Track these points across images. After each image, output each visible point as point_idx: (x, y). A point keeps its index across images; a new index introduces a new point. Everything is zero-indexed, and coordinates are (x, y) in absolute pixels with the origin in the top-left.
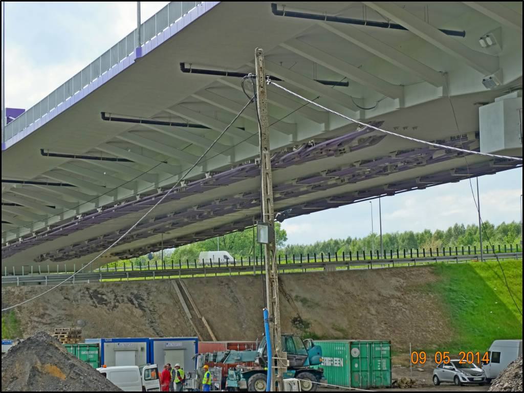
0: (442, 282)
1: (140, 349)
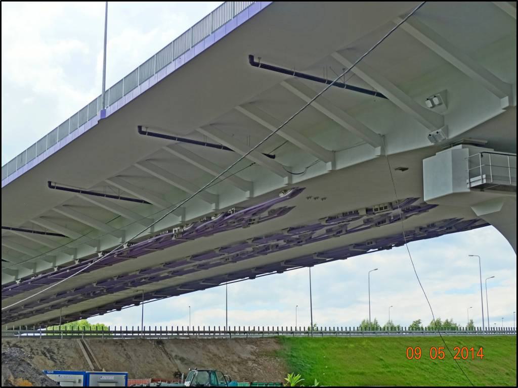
0: (285, 350)
1: (78, 381)
